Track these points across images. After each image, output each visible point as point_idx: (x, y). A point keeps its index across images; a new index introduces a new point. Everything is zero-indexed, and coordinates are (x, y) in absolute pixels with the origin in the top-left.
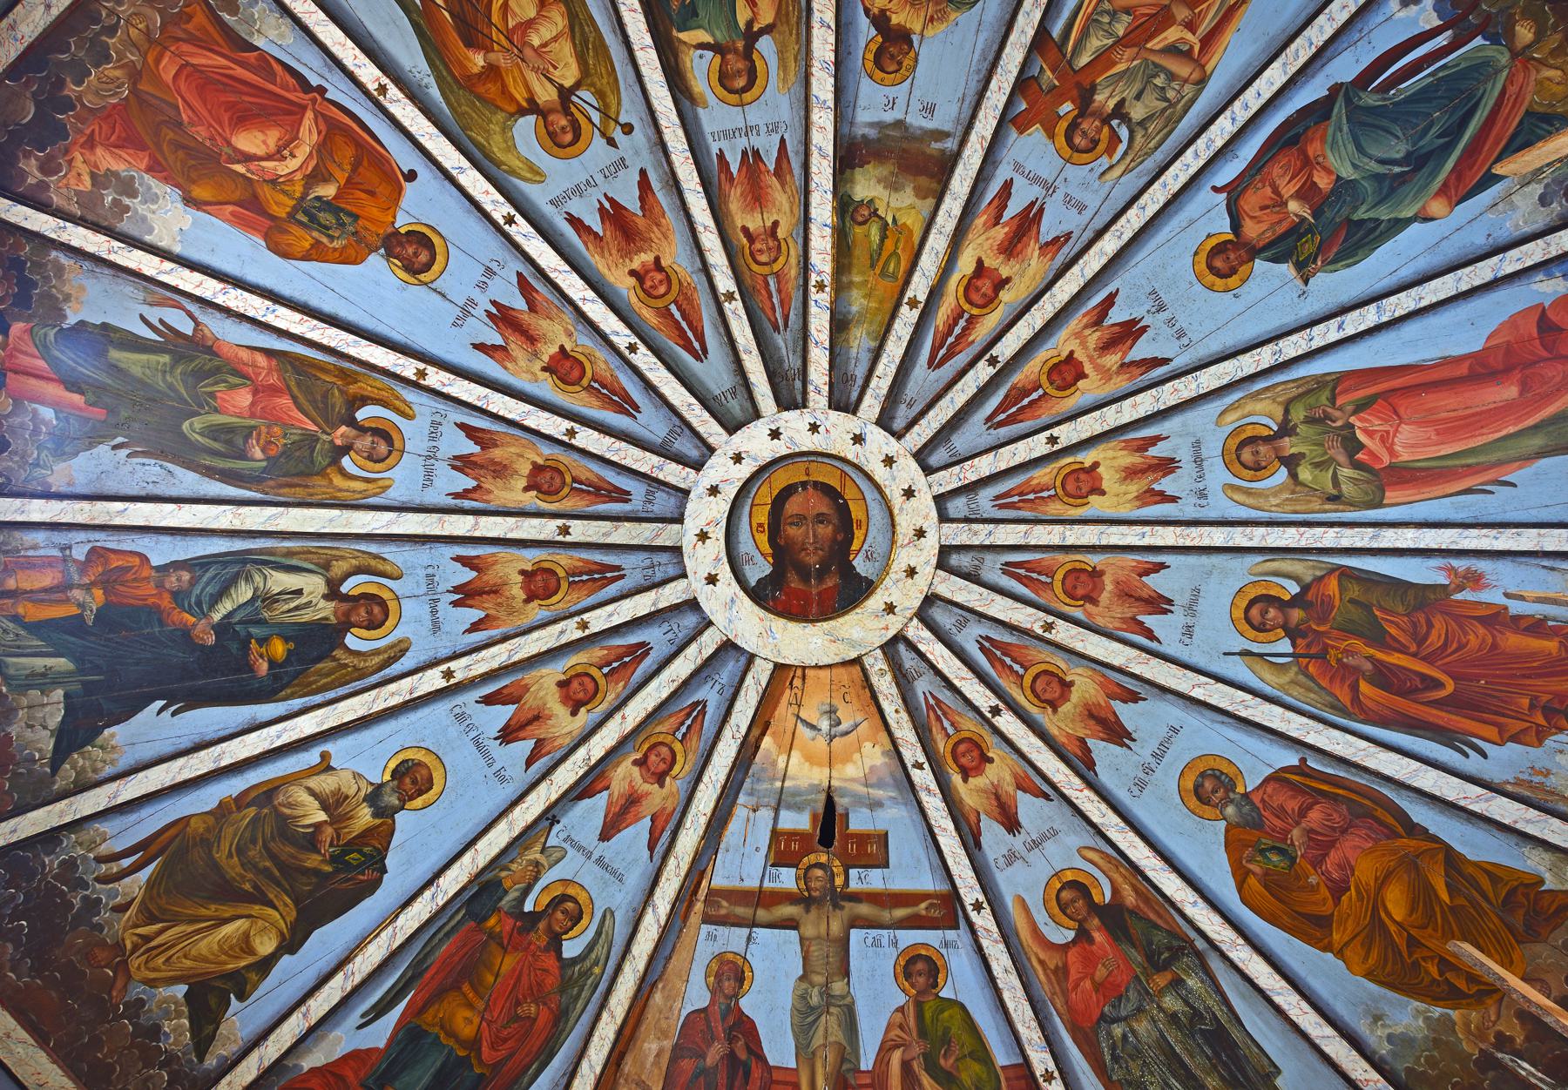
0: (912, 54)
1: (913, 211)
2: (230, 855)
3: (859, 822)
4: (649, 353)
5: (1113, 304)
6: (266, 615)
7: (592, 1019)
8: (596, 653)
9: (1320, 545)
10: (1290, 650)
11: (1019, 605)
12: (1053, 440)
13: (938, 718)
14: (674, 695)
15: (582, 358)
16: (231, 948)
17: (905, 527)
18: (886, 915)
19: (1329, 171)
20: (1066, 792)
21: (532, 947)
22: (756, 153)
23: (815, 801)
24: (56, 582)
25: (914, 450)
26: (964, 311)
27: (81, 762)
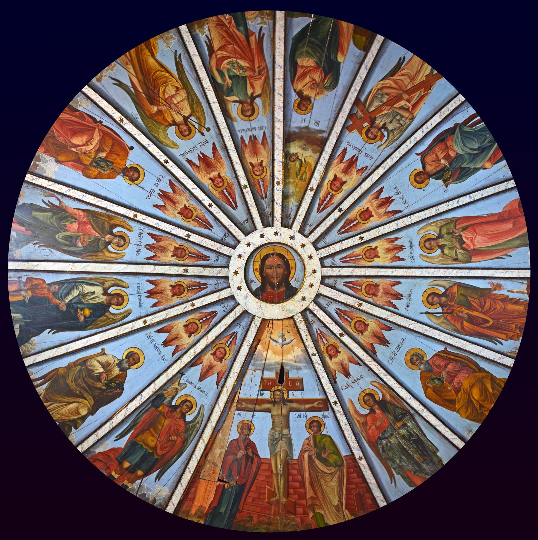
0: (311, 104)
1: (312, 157)
2: (72, 382)
3: (293, 375)
4: (216, 207)
5: (382, 191)
6: (83, 300)
7: (197, 442)
8: (197, 315)
9: (451, 275)
10: (442, 311)
11: (350, 297)
12: (361, 238)
13: (321, 338)
14: (225, 330)
15: (192, 209)
16: (72, 412)
17: (309, 269)
18: (302, 407)
19: (454, 151)
20: (366, 362)
21: (175, 417)
22: (255, 137)
23: (277, 368)
24: (17, 289)
25: (312, 242)
26: (330, 193)
27: (24, 348)
